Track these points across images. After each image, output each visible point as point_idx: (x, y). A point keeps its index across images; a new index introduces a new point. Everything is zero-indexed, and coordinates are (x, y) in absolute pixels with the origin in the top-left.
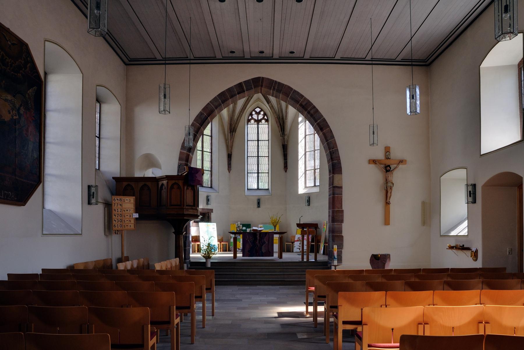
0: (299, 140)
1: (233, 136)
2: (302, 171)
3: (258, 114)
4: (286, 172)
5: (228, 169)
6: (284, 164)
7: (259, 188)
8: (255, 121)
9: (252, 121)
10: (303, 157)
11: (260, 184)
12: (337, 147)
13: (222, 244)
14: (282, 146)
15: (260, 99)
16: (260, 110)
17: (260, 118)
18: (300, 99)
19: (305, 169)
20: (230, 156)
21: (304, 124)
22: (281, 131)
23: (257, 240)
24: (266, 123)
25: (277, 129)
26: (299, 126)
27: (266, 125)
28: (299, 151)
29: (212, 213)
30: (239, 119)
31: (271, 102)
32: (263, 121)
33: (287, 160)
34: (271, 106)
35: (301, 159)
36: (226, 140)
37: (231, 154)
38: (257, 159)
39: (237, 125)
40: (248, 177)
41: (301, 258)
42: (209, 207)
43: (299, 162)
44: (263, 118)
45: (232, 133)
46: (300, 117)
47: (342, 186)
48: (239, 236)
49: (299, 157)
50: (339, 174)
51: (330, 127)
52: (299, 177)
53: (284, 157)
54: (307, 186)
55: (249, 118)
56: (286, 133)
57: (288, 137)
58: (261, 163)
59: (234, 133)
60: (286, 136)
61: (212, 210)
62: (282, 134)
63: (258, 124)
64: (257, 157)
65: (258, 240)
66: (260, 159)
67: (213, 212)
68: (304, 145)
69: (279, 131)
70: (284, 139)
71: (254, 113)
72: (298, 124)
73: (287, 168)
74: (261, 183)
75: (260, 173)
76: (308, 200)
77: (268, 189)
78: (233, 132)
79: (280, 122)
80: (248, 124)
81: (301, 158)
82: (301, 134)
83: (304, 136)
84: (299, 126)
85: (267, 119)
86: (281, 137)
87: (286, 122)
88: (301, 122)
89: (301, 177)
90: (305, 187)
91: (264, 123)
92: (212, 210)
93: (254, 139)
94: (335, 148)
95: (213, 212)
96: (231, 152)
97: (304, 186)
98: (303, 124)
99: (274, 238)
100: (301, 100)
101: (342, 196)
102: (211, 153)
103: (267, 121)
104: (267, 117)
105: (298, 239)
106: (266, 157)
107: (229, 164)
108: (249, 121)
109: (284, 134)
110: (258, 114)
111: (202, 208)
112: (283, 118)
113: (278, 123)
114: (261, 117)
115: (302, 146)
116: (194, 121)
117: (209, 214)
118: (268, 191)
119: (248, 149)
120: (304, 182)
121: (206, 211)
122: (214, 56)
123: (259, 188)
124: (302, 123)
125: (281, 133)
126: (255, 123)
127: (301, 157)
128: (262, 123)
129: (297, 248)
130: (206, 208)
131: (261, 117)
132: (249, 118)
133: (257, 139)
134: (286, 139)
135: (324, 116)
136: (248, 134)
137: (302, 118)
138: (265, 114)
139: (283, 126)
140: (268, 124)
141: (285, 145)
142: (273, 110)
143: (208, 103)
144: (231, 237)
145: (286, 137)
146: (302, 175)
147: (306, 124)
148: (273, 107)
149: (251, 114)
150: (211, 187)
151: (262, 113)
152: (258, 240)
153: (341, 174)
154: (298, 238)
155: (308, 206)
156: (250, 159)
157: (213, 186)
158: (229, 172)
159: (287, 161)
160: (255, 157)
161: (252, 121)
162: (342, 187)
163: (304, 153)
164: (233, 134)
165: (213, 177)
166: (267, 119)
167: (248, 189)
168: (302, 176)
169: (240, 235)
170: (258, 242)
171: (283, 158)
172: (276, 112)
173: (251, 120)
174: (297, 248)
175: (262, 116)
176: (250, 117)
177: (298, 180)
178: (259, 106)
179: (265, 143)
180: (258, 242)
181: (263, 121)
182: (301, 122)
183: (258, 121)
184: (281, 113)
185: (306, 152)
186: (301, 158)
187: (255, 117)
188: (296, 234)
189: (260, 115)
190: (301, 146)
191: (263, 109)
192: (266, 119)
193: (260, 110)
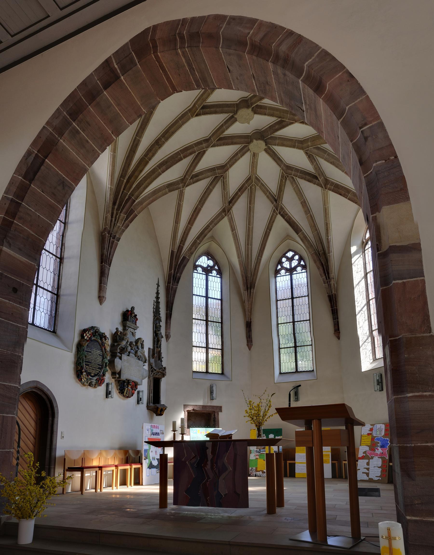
0: (355, 282)
1: (251, 294)
2: (365, 332)
3: (290, 260)
4: (339, 338)
5: (248, 345)
6: (335, 327)
7: (299, 370)
8: (287, 270)
9: (283, 272)
10: (364, 310)
11: (300, 363)
12: (378, 117)
13: (134, 468)
14: (327, 299)
15: (292, 237)
16: (293, 253)
17: (293, 266)
18: (247, 31)
19: (369, 329)
20: (249, 325)
21: (362, 256)
22: (323, 275)
23: (207, 461)
24: (304, 271)
25: (317, 272)
26: (352, 259)
27: (303, 274)
28: (356, 300)
29: (220, 413)
30: (257, 267)
31: (302, 230)
32: (299, 269)
33: (338, 319)
34: (302, 236)
35: (362, 312)
36: (243, 303)
37: (251, 322)
38: (292, 326)
39: (255, 277)
40: (280, 354)
41: (308, 527)
42: (215, 403)
43: (358, 317)
44: (299, 265)
45: (249, 290)
46: (353, 246)
47: (417, 242)
48: (264, 450)
49: (357, 309)
50: (396, 201)
51: (344, 67)
52: (361, 343)
53: (333, 316)
54: (377, 358)
55: (278, 269)
56: (331, 275)
57: (337, 283)
58: (298, 332)
59: (252, 289)
60: (332, 280)
61: (220, 409)
62: (327, 279)
63: (291, 275)
64: (292, 323)
65: (209, 463)
66: (298, 325)
67: (221, 411)
68: (364, 289)
69: (321, 275)
70: (330, 285)
71: (284, 260)
72: (350, 257)
73: (339, 332)
74: (300, 362)
75: (298, 346)
76: (380, 381)
77: (313, 371)
78: (250, 289)
79: (320, 260)
80: (276, 277)
81: (361, 310)
82: (357, 273)
83: (363, 275)
84: (353, 260)
85: (304, 264)
86: (324, 283)
87: (330, 256)
88: (356, 253)
89: (365, 342)
90: (374, 360)
91: (300, 272)
92: (220, 409)
93: (286, 297)
94: (370, 122)
95: (221, 411)
96: (251, 320)
97: (371, 358)
98: (360, 257)
99: (323, 453)
100: (249, 33)
101: (423, 282)
102: (222, 323)
103: (304, 267)
104: (304, 262)
105: (365, 455)
106: (306, 322)
107: (248, 336)
108: (277, 272)
109: (329, 278)
110: (290, 260)
111: (202, 405)
112: (325, 253)
113: (318, 262)
114: (294, 263)
115: (361, 291)
116: (14, 173)
117: (214, 415)
118: (312, 373)
119: (279, 313)
120: (371, 351)
121: (210, 410)
122: (43, 16)
123: (299, 370)
124: (358, 255)
125: (324, 277)
126: (287, 274)
127: (360, 309)
128: (297, 272)
129: (363, 473)
130: (209, 404)
131: (294, 263)
132: (278, 269)
133: (291, 296)
134: (333, 284)
135: (320, 45)
136: (278, 292)
137: (357, 247)
138: (301, 258)
139: (326, 269)
140: (307, 272)
141: (332, 295)
142: (306, 243)
143: (44, 127)
144: (251, 450)
145: (332, 282)
146: (366, 338)
147: (365, 255)
148: (305, 237)
149: (280, 262)
150: (222, 373)
151: (297, 257)
152: (209, 463)
153: (407, 198)
154: (363, 453)
155: (380, 391)
156: (281, 327)
157: (225, 372)
158: (250, 349)
159: (338, 322)
160: (290, 322)
161: (283, 272)
162: (420, 244)
163: (365, 302)
164: (252, 291)
165: (225, 358)
166: (304, 264)
167: (280, 373)
168: (367, 341)
169: (264, 448)
170: (209, 467)
171: (332, 317)
172: (311, 246)
173: (280, 270)
174: (363, 473)
175: (297, 261)
176: (279, 267)
177: (359, 348)
178: (291, 249)
179: (304, 300)
180: (209, 467)
181: (299, 269)
182: (356, 253)
183: (291, 271)
184: (320, 245)
185: (369, 300)
186: (361, 310)
187: (286, 265)
188: (360, 445)
189: (294, 261)
190: (359, 291)
191: (297, 250)
192: (302, 265)
193: (293, 253)
